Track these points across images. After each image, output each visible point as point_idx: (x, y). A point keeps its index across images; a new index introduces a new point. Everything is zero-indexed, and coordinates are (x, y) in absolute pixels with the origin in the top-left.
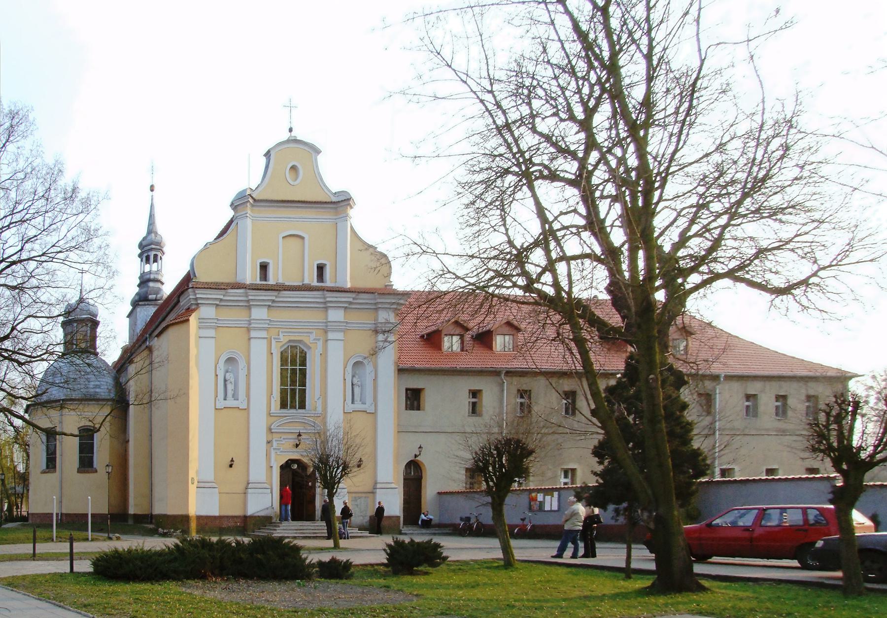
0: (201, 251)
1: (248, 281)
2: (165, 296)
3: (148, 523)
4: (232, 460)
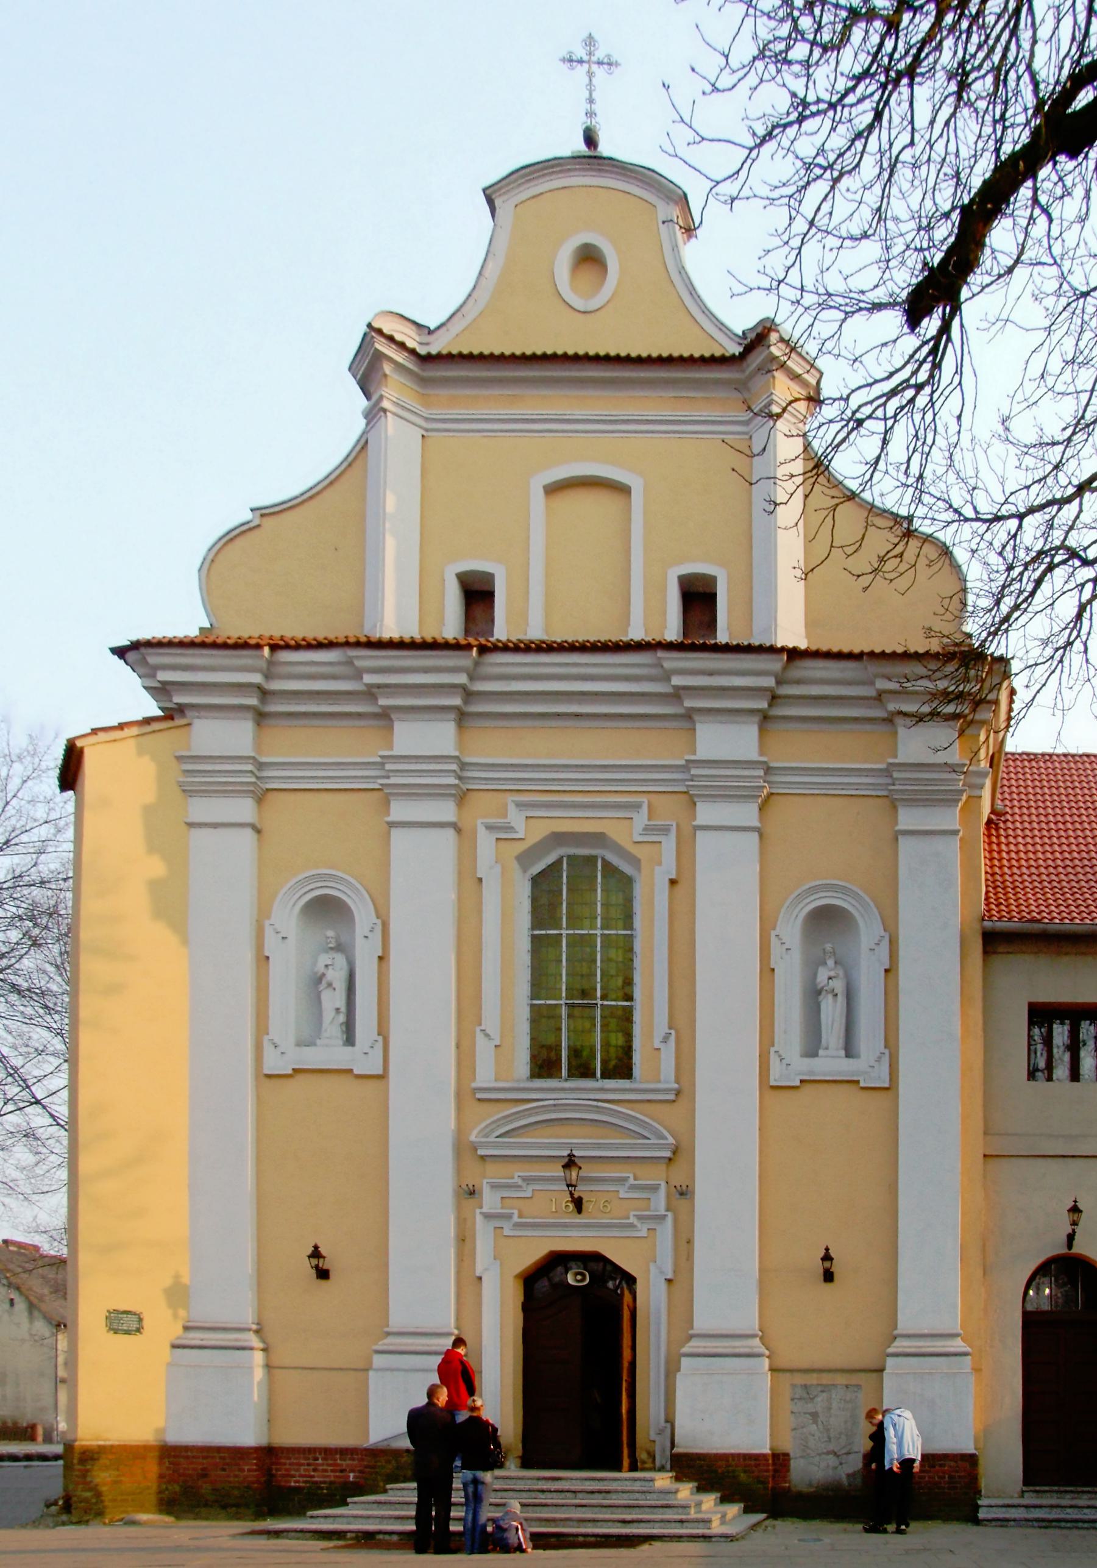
1: (390, 630)
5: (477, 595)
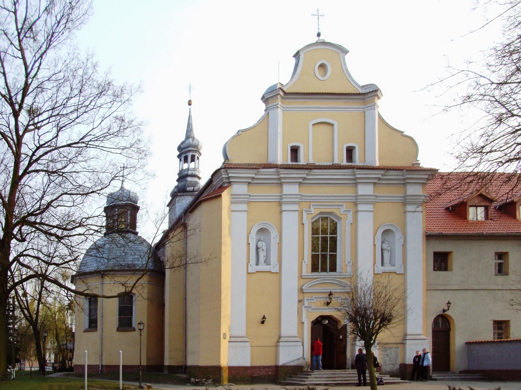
0: (233, 137)
1: (280, 162)
2: (201, 187)
3: (182, 373)
4: (264, 317)
5: (295, 151)
